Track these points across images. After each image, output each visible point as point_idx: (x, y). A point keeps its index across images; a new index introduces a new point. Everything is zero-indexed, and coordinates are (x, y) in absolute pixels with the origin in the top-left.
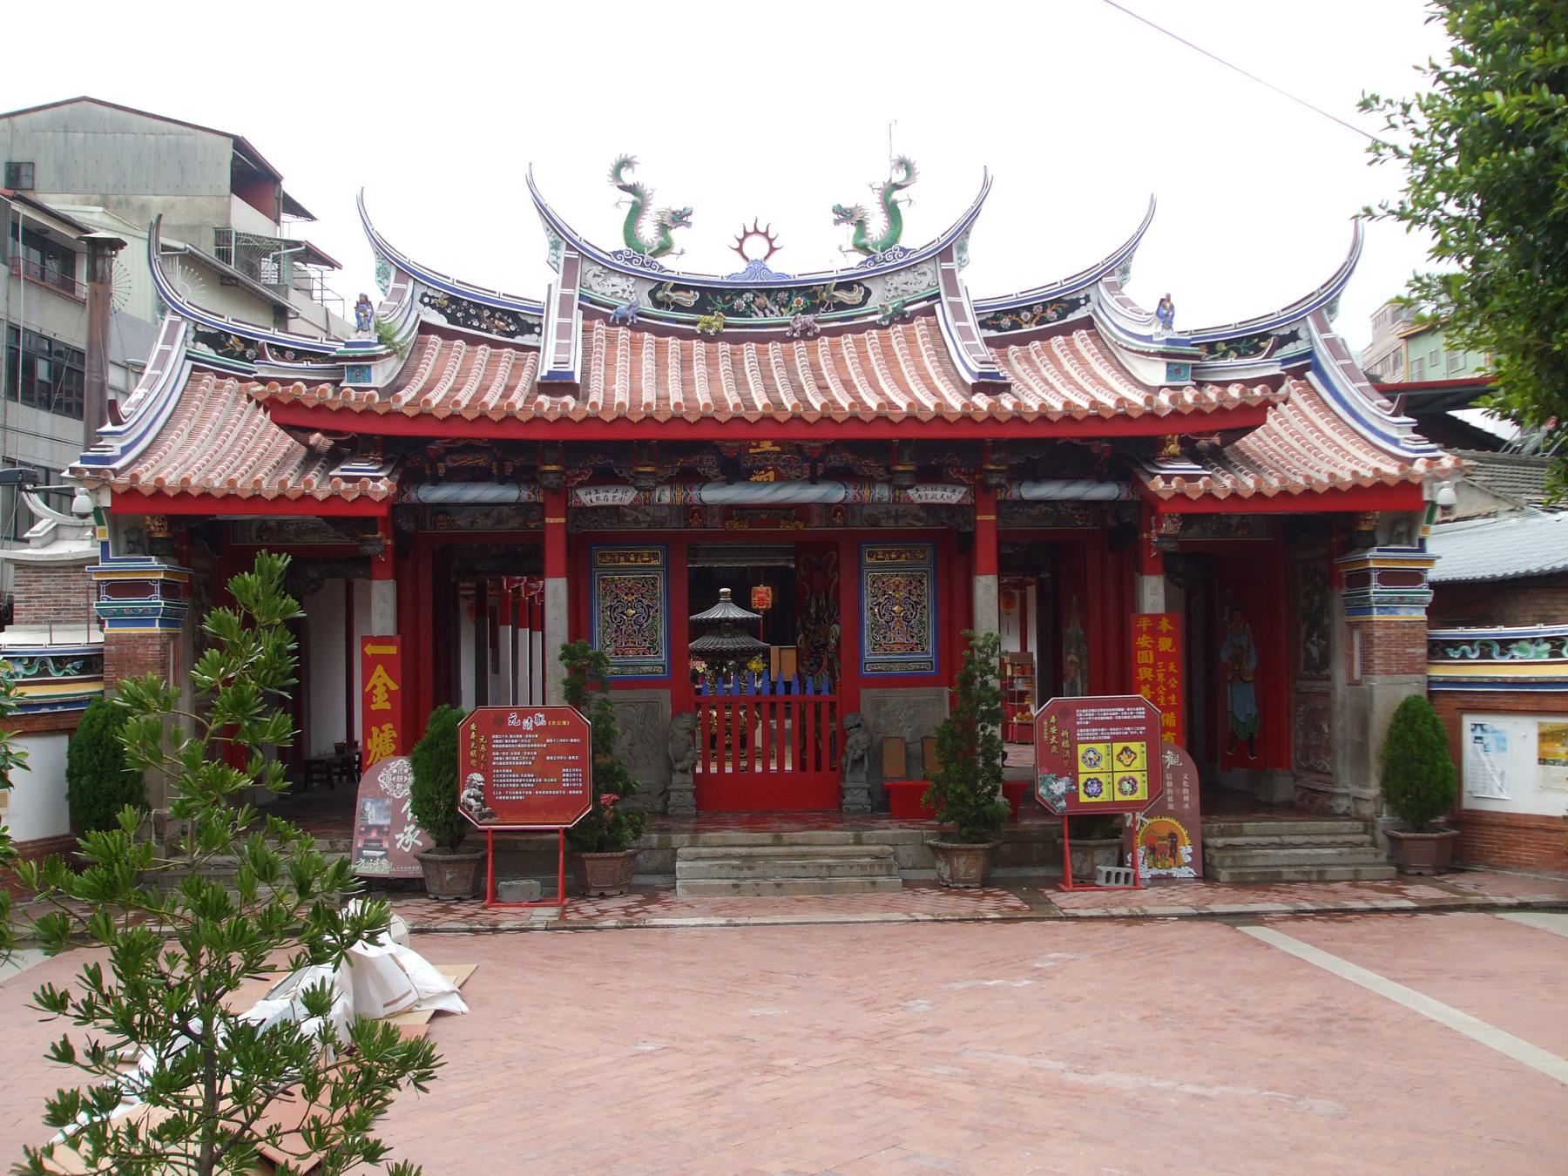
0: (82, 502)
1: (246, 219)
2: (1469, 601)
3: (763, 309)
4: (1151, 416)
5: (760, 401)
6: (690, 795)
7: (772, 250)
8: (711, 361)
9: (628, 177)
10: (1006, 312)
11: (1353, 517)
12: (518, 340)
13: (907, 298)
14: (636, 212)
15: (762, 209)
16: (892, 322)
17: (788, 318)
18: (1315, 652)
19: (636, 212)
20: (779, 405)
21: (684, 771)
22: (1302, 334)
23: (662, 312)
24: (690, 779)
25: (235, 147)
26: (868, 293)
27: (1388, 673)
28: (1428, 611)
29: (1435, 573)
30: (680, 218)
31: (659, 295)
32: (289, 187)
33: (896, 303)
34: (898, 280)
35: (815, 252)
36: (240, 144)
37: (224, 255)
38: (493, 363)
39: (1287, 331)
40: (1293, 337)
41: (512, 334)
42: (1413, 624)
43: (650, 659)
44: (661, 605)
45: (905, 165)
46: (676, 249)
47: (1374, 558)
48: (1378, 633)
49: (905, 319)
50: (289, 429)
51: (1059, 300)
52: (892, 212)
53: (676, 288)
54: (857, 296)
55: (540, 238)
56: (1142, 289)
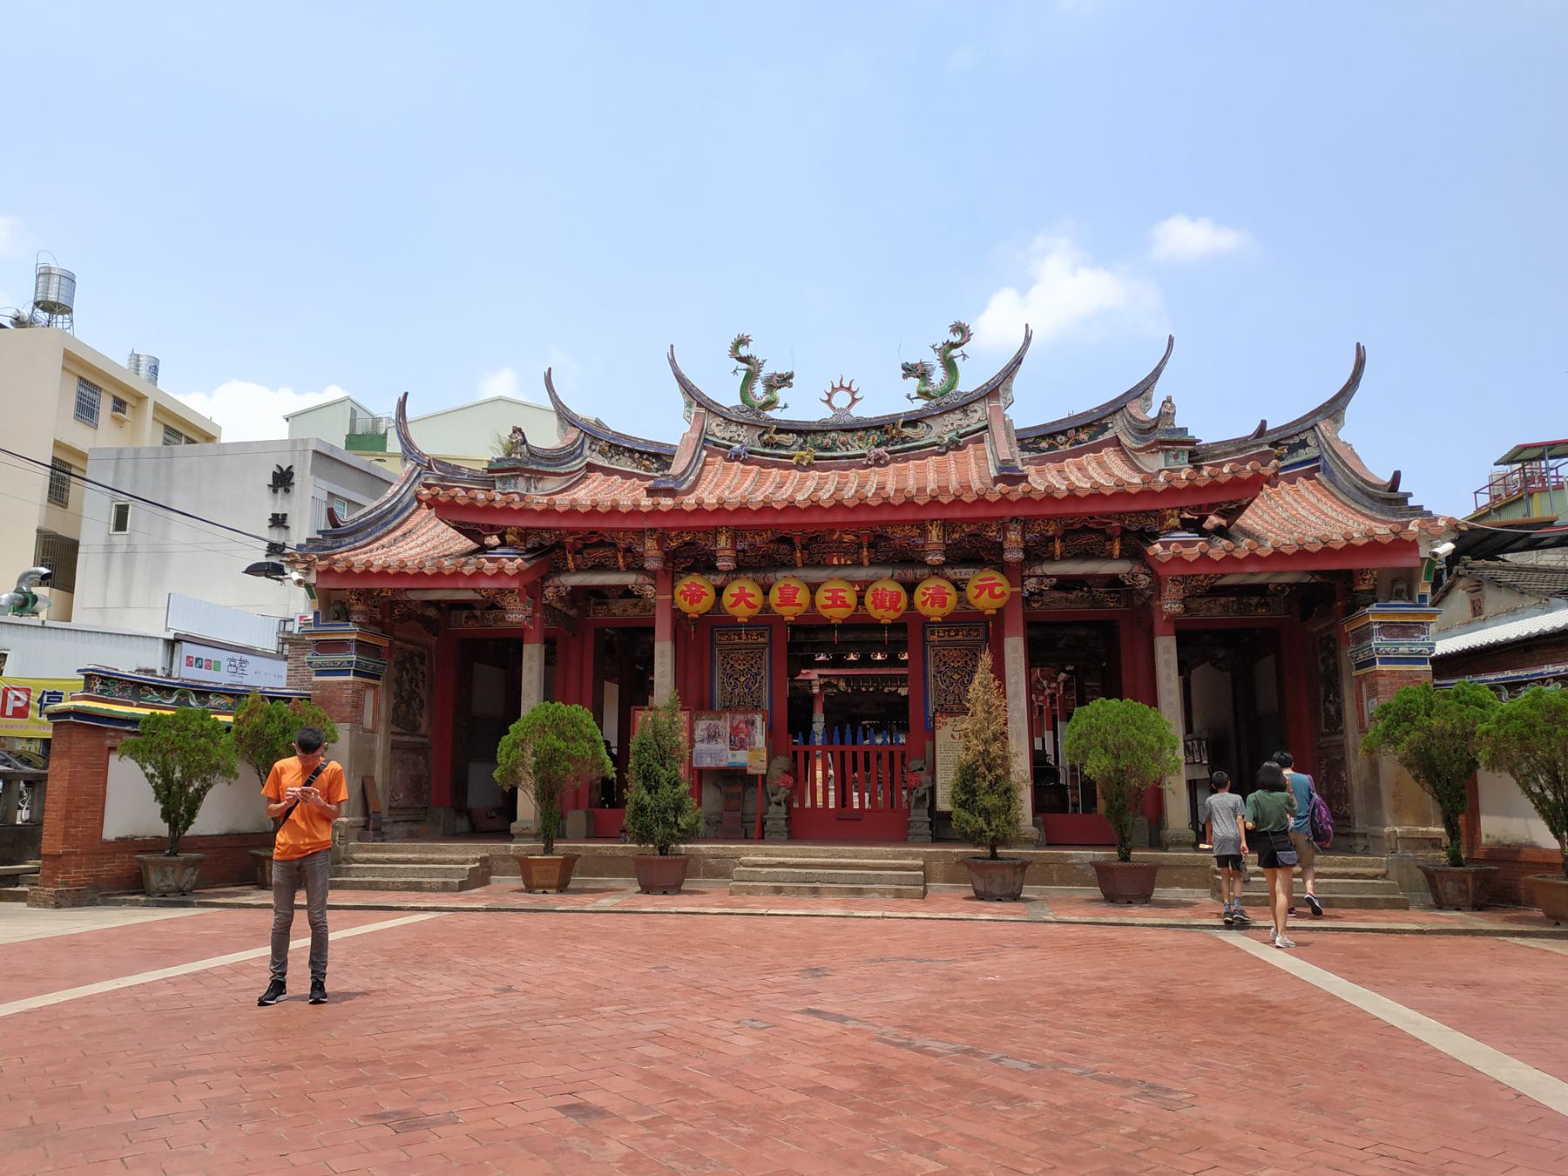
4: (1147, 493)
6: (783, 823)
7: (854, 400)
9: (743, 351)
10: (1043, 437)
11: (1349, 576)
14: (750, 377)
15: (847, 365)
16: (948, 449)
18: (1332, 710)
21: (779, 804)
22: (1311, 441)
24: (783, 809)
30: (785, 380)
35: (889, 397)
39: (1297, 440)
40: (1304, 444)
44: (765, 673)
45: (959, 328)
46: (781, 404)
48: (1381, 681)
50: (462, 528)
53: (779, 431)
55: (678, 398)
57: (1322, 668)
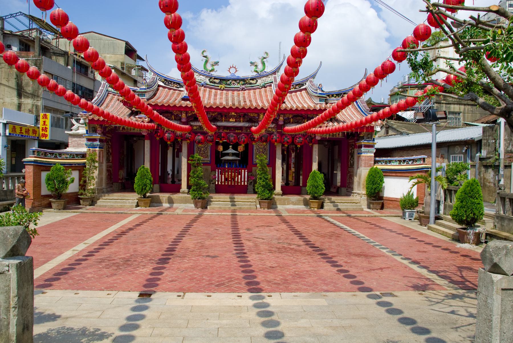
0: (82, 121)
1: (129, 61)
2: (382, 153)
3: (234, 84)
5: (261, 105)
7: (236, 71)
8: (221, 94)
12: (180, 89)
13: (266, 83)
14: (207, 62)
17: (239, 86)
19: (207, 62)
20: (259, 105)
23: (212, 84)
24: (214, 185)
25: (126, 44)
26: (257, 81)
27: (365, 167)
28: (374, 154)
29: (377, 146)
30: (216, 63)
31: (211, 80)
32: (138, 53)
33: (263, 83)
34: (264, 79)
36: (127, 43)
37: (123, 68)
38: (173, 94)
41: (178, 88)
42: (371, 156)
43: (206, 159)
47: (363, 142)
49: (265, 87)
51: (299, 84)
52: (263, 63)
53: (215, 79)
54: (254, 82)
56: (316, 82)
57: (350, 151)
